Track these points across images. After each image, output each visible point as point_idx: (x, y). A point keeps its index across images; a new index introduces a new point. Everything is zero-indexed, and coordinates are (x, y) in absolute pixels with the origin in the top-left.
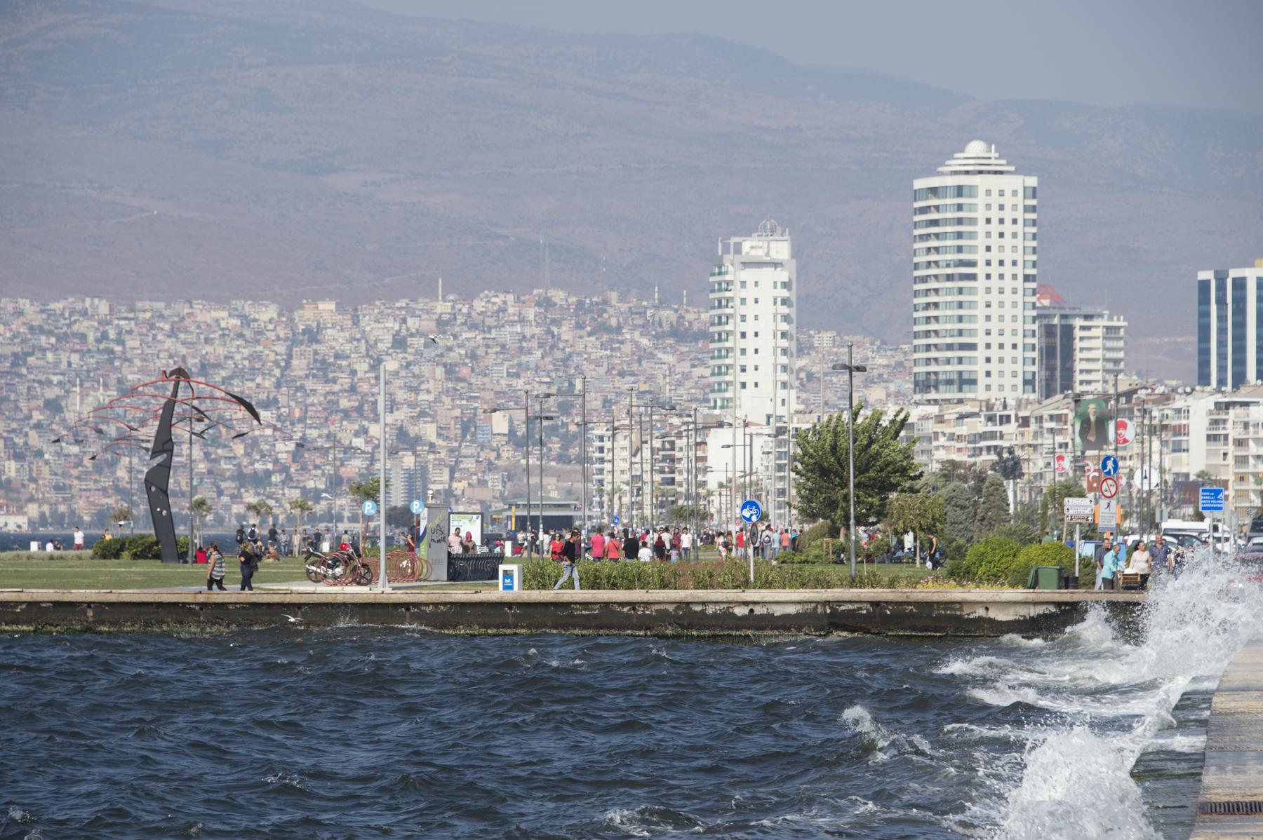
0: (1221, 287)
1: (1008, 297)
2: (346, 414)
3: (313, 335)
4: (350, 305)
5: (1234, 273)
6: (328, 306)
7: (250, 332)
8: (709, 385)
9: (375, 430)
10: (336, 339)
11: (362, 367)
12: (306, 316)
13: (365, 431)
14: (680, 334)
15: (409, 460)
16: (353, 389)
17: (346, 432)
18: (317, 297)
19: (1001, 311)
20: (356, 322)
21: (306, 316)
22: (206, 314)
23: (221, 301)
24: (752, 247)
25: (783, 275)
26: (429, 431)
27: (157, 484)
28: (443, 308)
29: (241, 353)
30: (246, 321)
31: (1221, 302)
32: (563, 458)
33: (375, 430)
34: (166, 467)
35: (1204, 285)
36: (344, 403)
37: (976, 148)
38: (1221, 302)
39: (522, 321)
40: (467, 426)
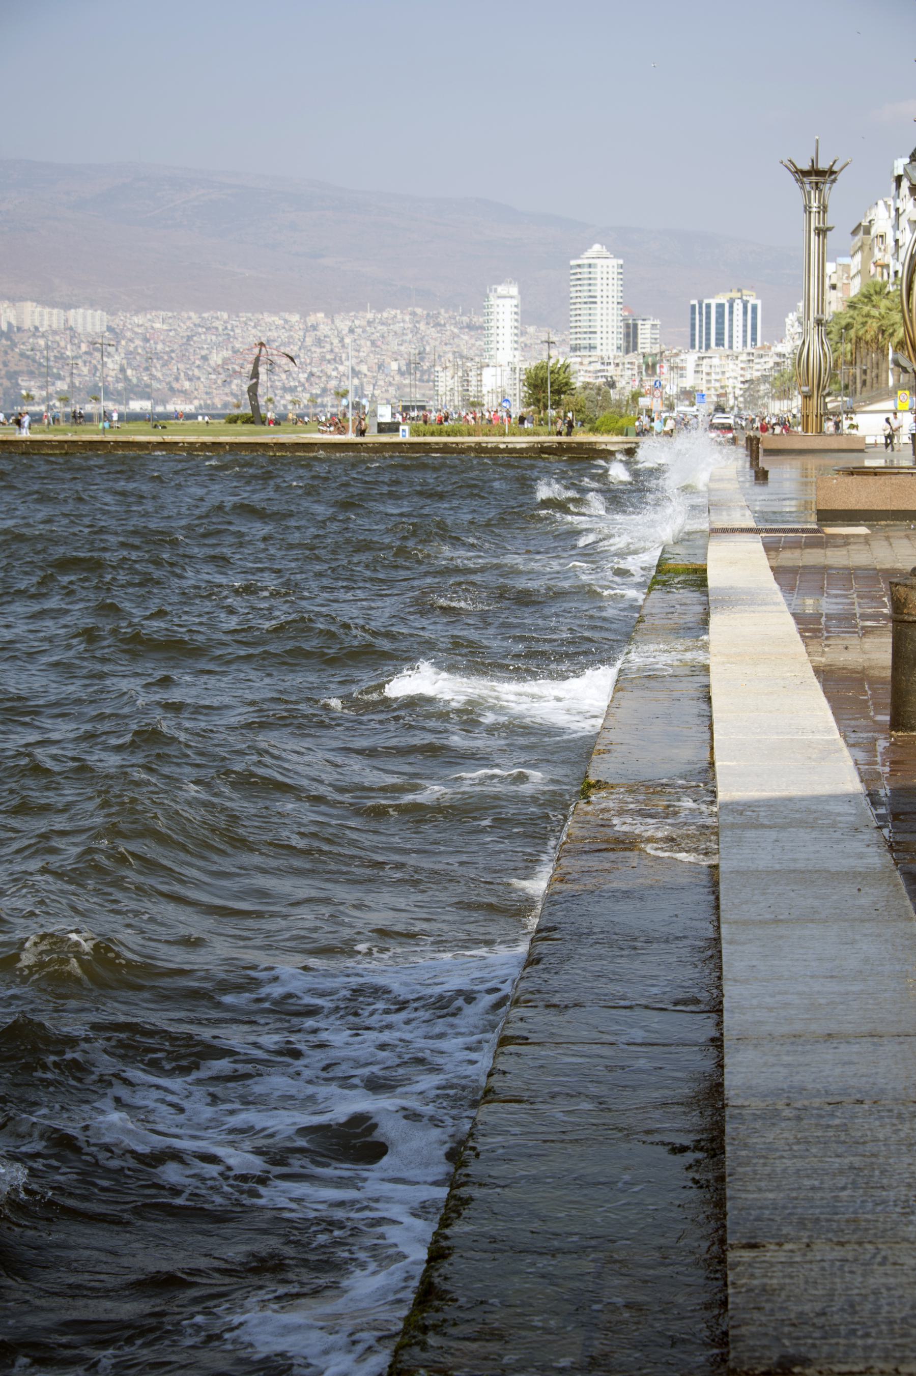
0: (701, 307)
1: (610, 311)
2: (329, 362)
3: (315, 328)
4: (330, 314)
5: (706, 301)
6: (321, 315)
7: (288, 326)
9: (341, 368)
10: (324, 329)
11: (336, 341)
12: (311, 320)
13: (336, 369)
14: (470, 327)
16: (332, 351)
18: (316, 311)
20: (333, 322)
21: (311, 320)
22: (268, 318)
23: (276, 313)
24: (501, 289)
27: (253, 391)
29: (284, 335)
30: (286, 321)
31: (701, 313)
32: (421, 380)
34: (256, 384)
35: (693, 307)
36: (328, 357)
39: (404, 321)
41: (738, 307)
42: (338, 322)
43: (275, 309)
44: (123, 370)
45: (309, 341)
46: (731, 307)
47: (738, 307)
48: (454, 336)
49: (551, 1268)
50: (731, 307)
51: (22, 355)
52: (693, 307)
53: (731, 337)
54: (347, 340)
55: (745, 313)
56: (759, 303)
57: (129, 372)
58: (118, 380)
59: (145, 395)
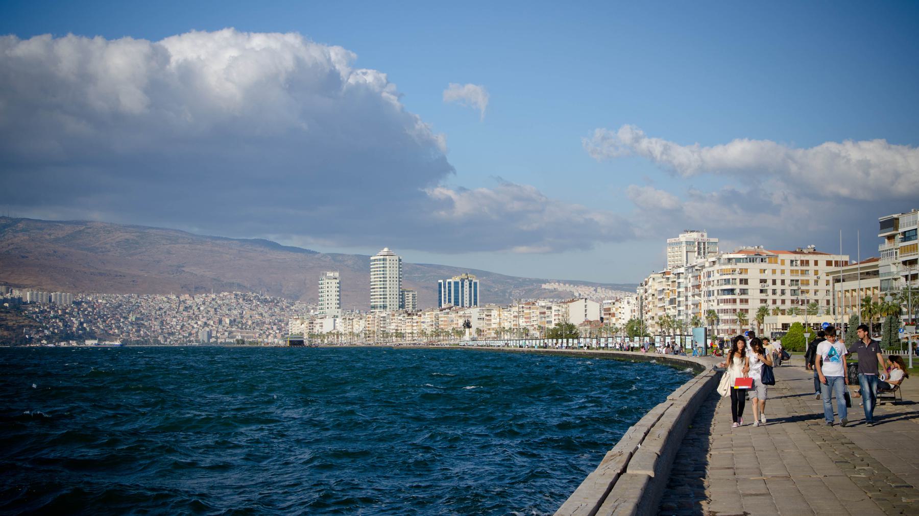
0: (445, 284)
3: (184, 302)
7: (169, 301)
8: (533, 363)
10: (189, 303)
11: (196, 309)
12: (182, 298)
15: (208, 329)
17: (193, 323)
18: (185, 293)
19: (774, 297)
21: (182, 298)
22: (159, 297)
25: (338, 281)
26: (212, 323)
28: (213, 296)
29: (168, 305)
31: (445, 287)
32: (242, 328)
33: (199, 323)
35: (440, 284)
37: (386, 250)
38: (445, 287)
40: (220, 321)
41: (467, 283)
42: (196, 300)
43: (163, 293)
44: (81, 324)
45: (181, 308)
46: (463, 284)
47: (467, 283)
48: (257, 306)
49: (82, 485)
50: (463, 284)
51: (26, 316)
52: (440, 284)
53: (463, 299)
54: (202, 308)
55: (470, 287)
56: (478, 281)
57: (85, 325)
58: (78, 329)
59: (92, 336)
